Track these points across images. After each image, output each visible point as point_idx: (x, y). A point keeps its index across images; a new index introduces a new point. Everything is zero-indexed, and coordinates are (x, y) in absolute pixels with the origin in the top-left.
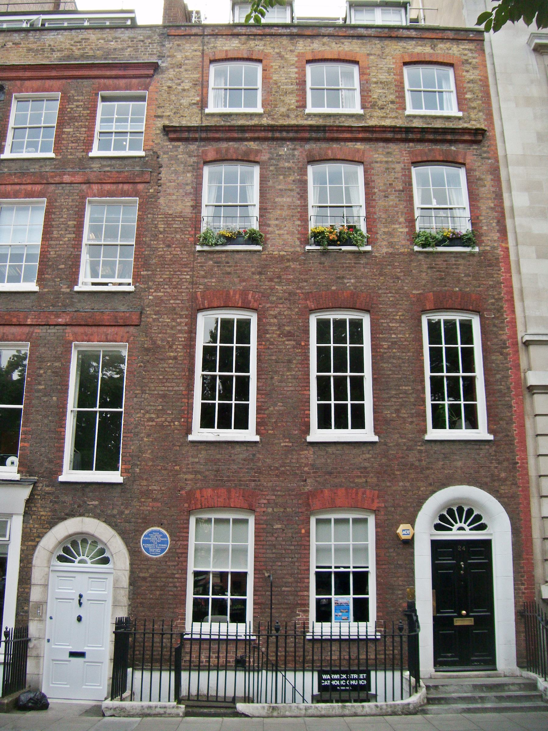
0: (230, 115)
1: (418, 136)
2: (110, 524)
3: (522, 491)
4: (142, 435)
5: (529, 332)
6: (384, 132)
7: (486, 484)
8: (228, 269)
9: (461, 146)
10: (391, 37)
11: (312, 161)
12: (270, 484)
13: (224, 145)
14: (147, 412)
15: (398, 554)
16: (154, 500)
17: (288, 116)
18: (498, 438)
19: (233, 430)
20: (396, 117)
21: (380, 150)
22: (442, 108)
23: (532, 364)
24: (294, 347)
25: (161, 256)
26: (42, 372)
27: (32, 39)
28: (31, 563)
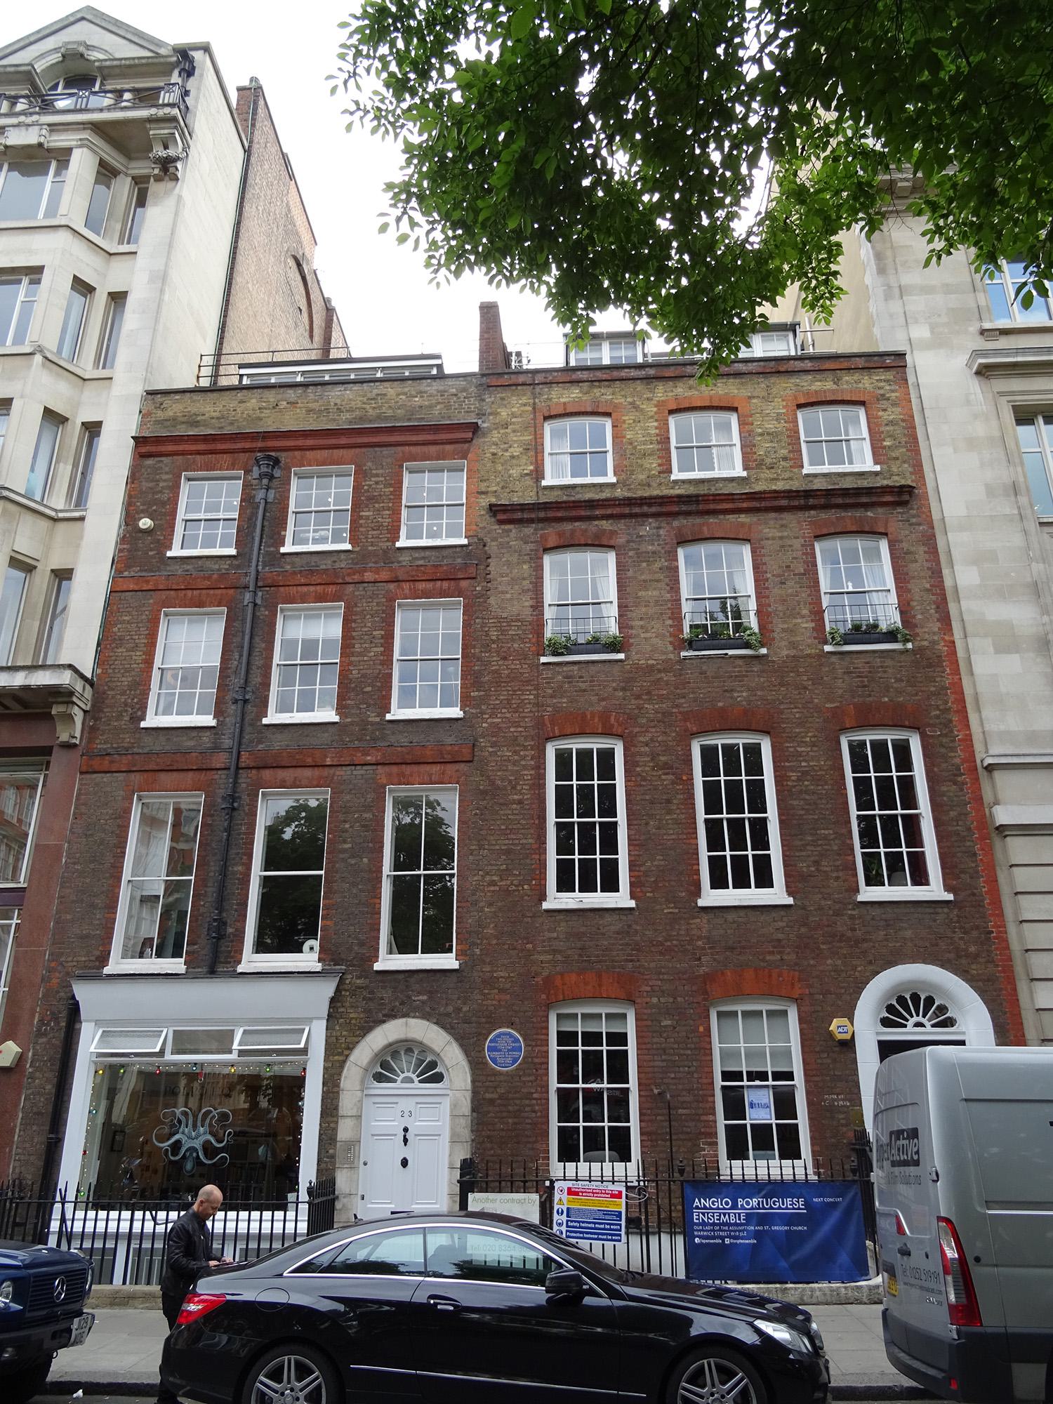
0: (574, 487)
1: (822, 501)
2: (443, 1027)
3: (1004, 971)
4: (481, 904)
5: (991, 752)
6: (776, 498)
7: (949, 961)
8: (583, 686)
9: (880, 510)
10: (779, 372)
11: (683, 542)
12: (653, 965)
13: (568, 527)
14: (487, 874)
15: (834, 1061)
16: (501, 991)
17: (649, 485)
18: (960, 898)
19: (599, 894)
20: (791, 479)
21: (772, 522)
22: (851, 462)
23: (1001, 796)
24: (673, 783)
25: (496, 672)
26: (347, 826)
27: (312, 396)
28: (338, 1086)
